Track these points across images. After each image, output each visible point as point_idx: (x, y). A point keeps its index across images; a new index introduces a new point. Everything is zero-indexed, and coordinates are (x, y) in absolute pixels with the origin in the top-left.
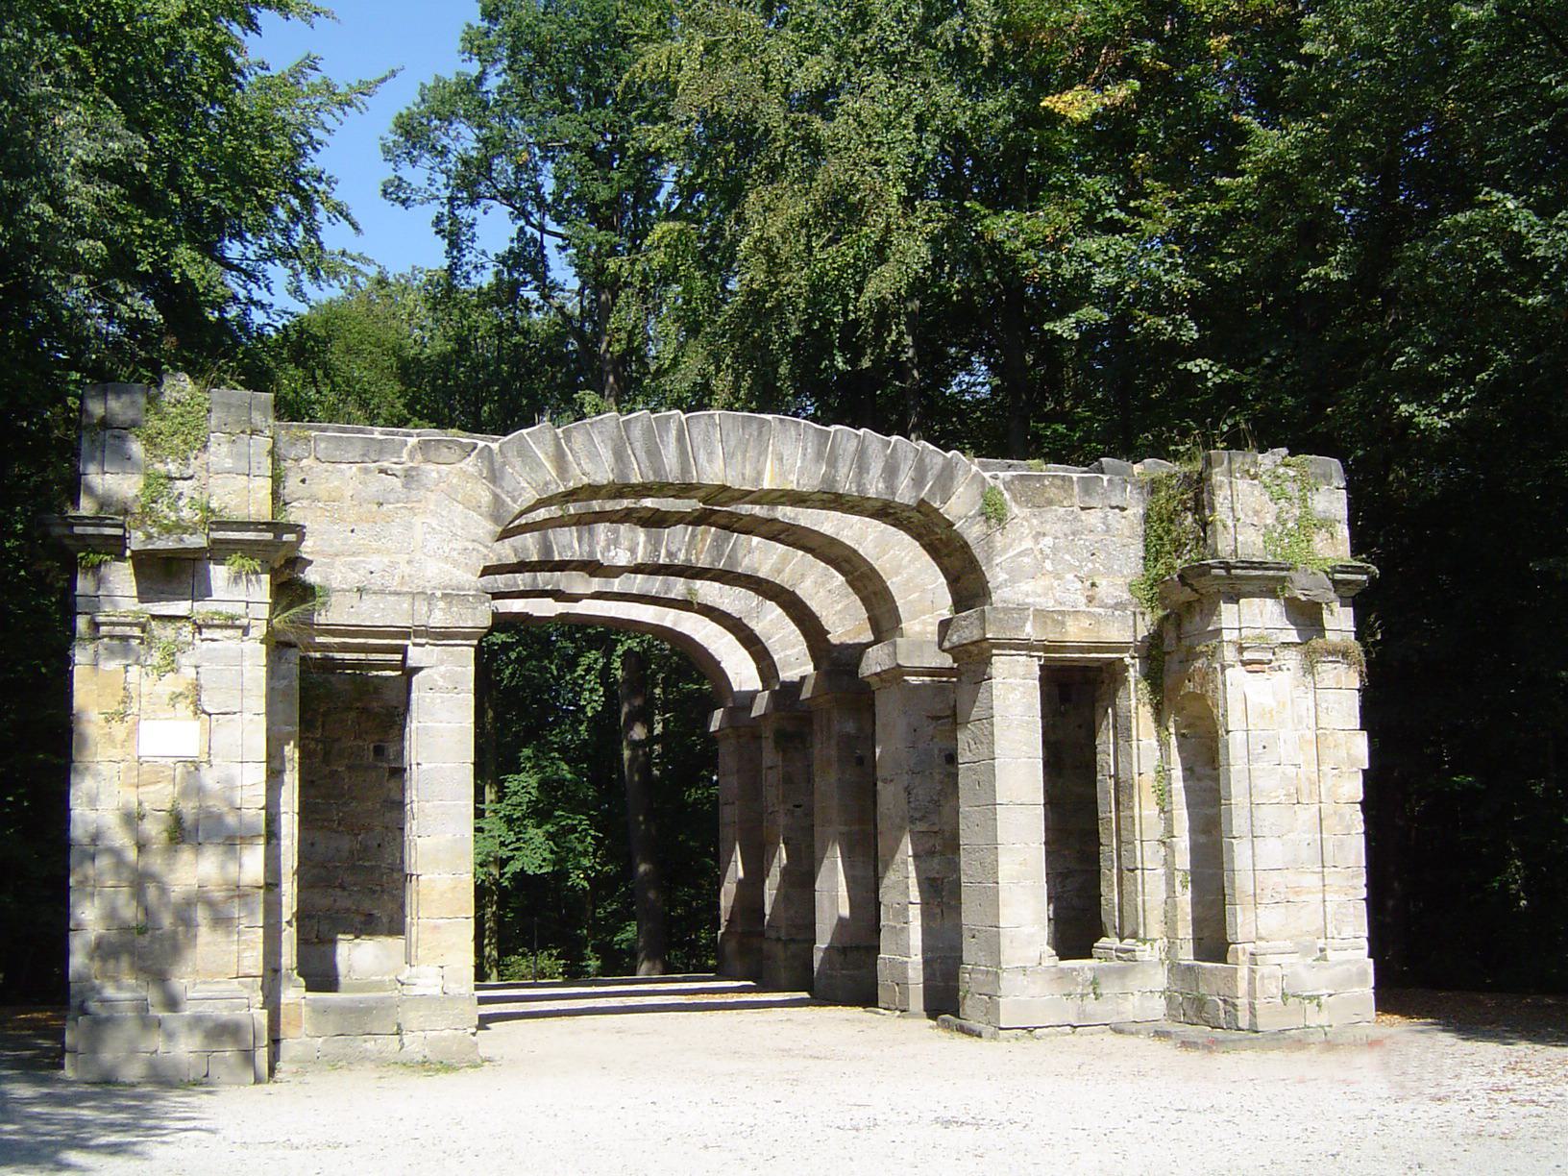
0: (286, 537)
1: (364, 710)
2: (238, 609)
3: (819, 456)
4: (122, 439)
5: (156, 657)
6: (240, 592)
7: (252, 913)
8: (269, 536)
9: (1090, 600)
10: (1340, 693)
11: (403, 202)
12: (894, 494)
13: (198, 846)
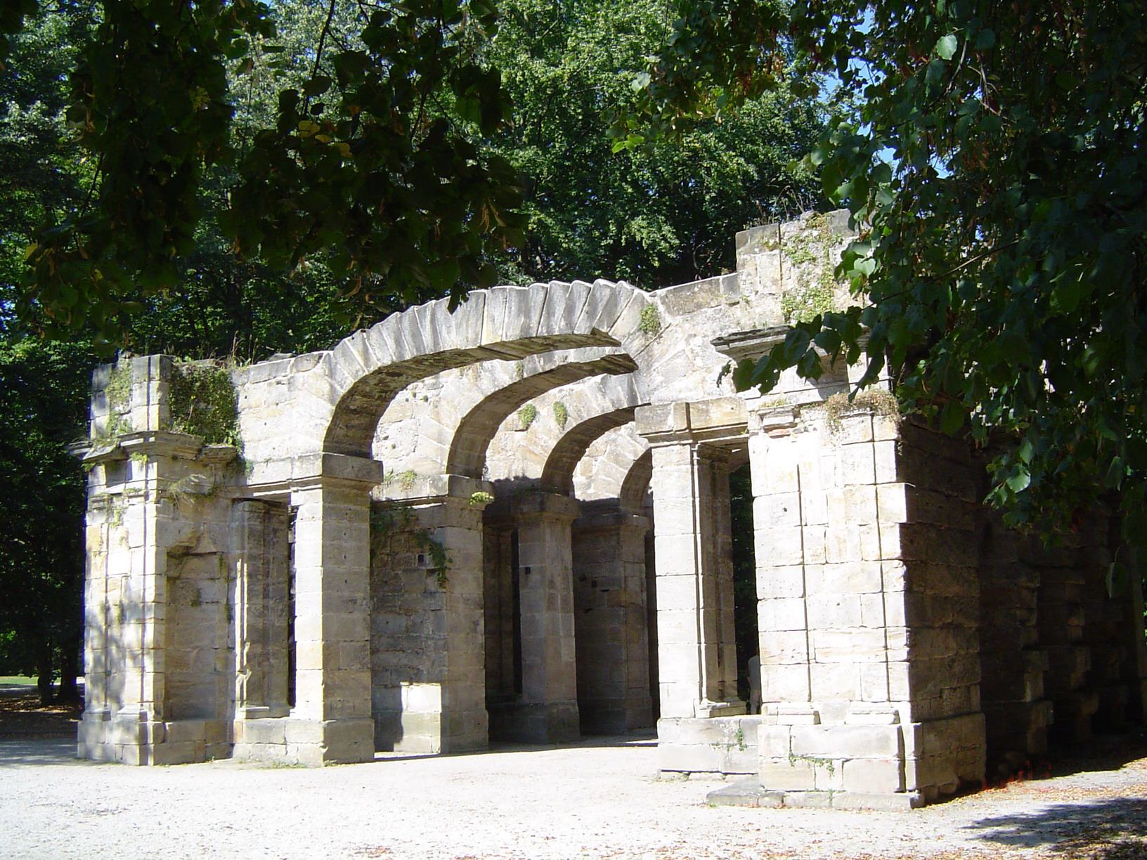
1: (411, 532)
3: (519, 311)
12: (572, 328)
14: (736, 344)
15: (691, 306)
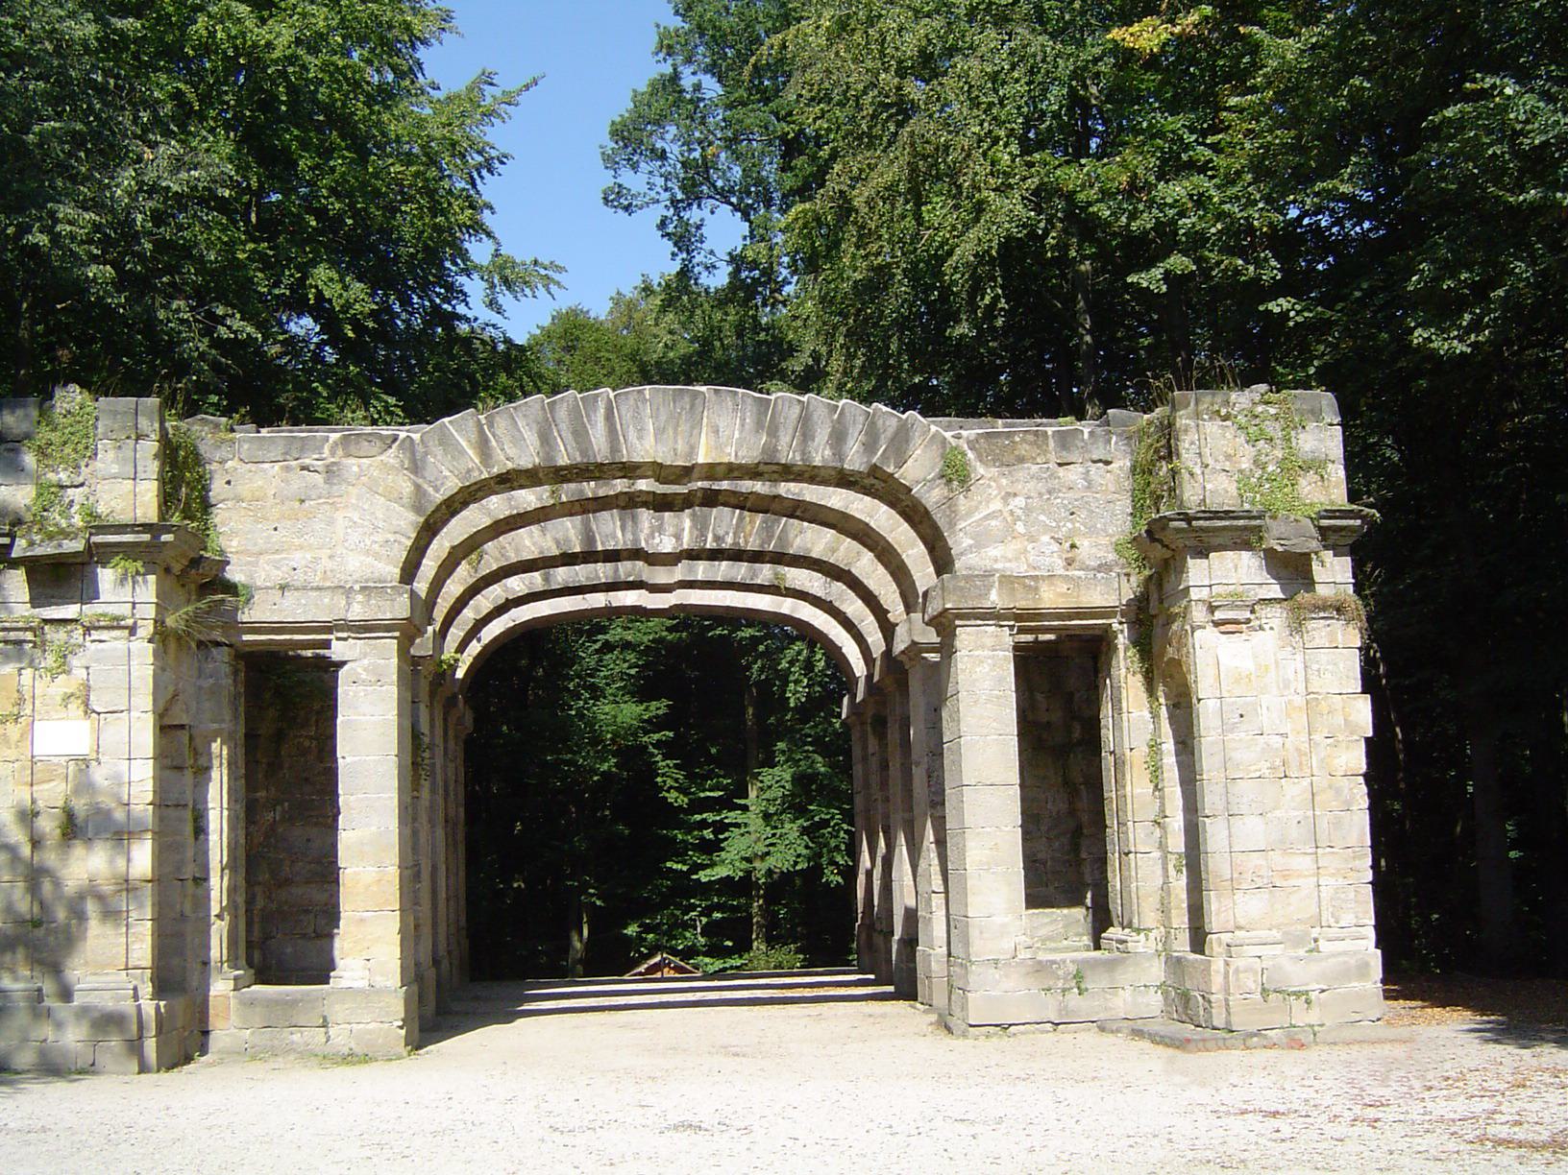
0: (165, 538)
2: (126, 610)
3: (759, 425)
4: (16, 451)
5: (50, 660)
6: (126, 594)
7: (141, 906)
8: (146, 537)
9: (1069, 562)
10: (1336, 655)
11: (626, 208)
12: (842, 460)
13: (89, 841)
14: (1201, 523)
15: (1008, 458)
